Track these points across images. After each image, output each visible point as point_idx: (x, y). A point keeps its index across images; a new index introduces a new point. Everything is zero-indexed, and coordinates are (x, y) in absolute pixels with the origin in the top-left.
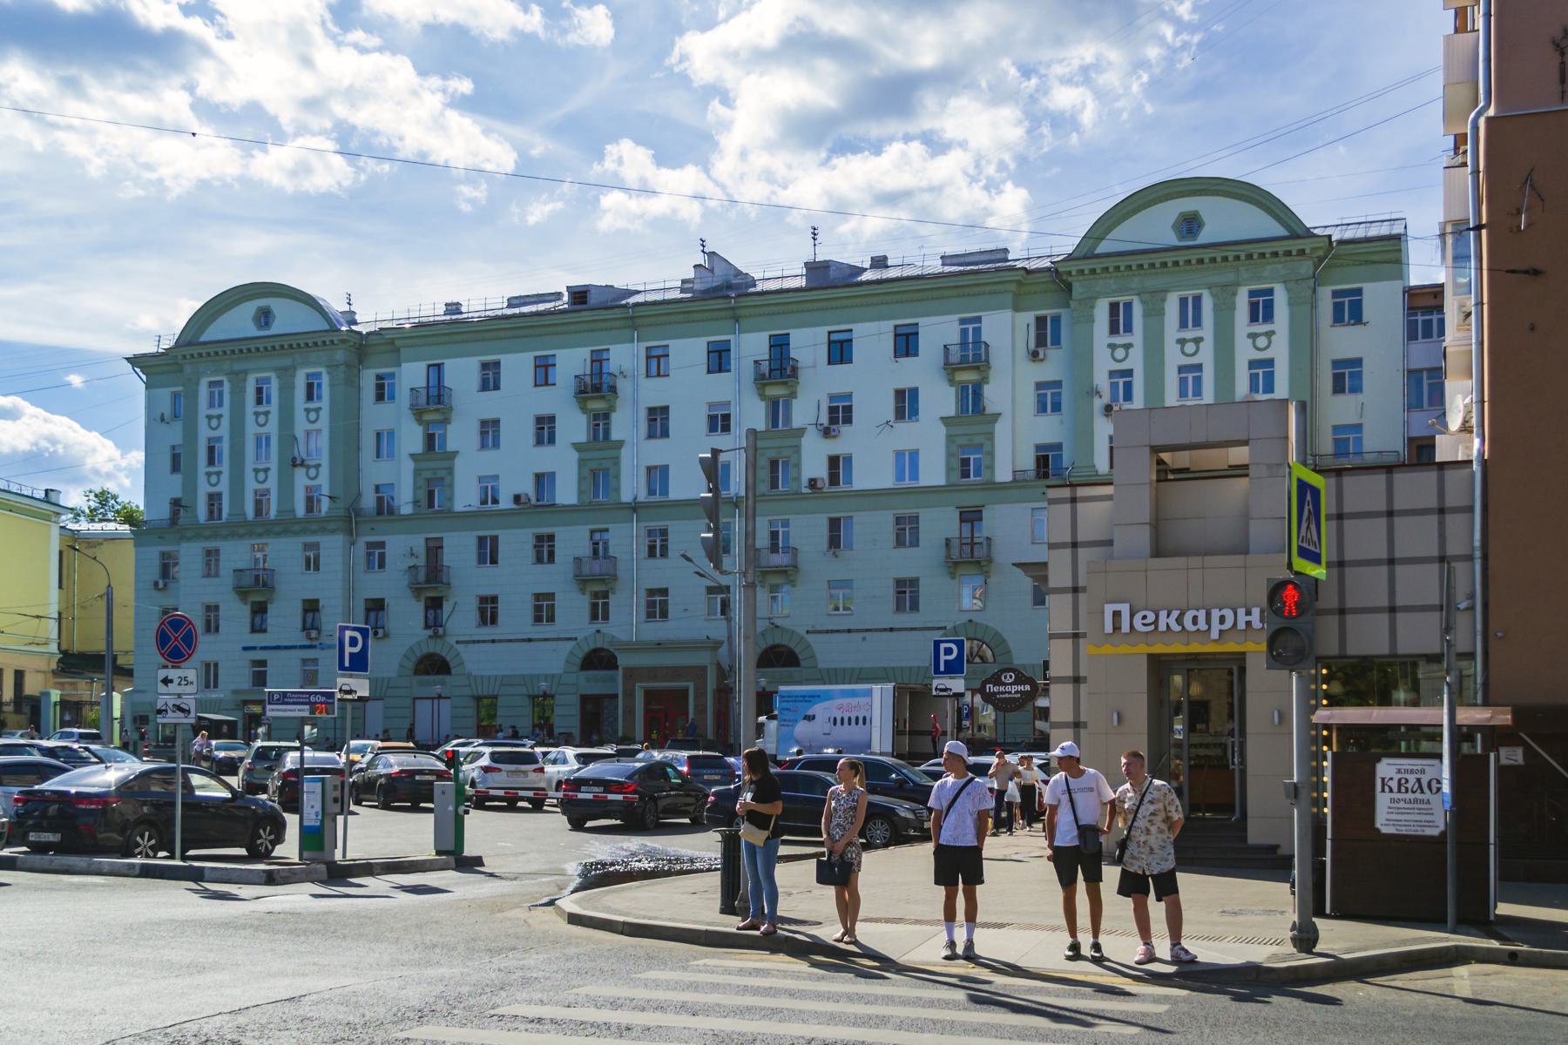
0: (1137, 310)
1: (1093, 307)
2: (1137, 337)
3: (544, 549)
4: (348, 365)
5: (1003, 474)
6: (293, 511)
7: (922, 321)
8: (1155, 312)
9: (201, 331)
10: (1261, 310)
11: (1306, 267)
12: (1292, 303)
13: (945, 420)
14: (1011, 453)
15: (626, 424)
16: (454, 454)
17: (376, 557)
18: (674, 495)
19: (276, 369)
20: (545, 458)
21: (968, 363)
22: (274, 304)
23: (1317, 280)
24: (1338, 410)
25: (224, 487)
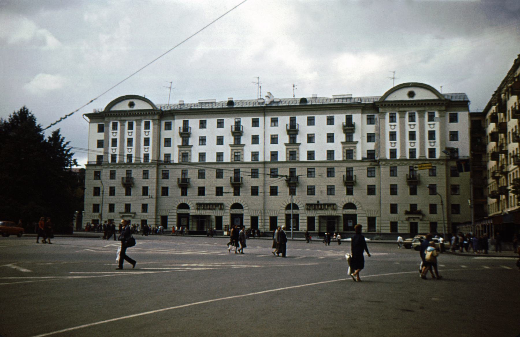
0: (417, 115)
1: (385, 115)
2: (398, 123)
3: (113, 175)
4: (159, 120)
5: (359, 157)
6: (108, 161)
7: (335, 115)
8: (123, 125)
9: (111, 108)
10: (147, 126)
11: (156, 117)
12: (154, 125)
13: (286, 144)
14: (360, 154)
15: (193, 141)
16: (191, 146)
17: (166, 176)
18: (207, 161)
19: (418, 111)
20: (220, 149)
21: (349, 128)
22: (135, 101)
23: (160, 120)
24: (165, 150)
25: (117, 152)
